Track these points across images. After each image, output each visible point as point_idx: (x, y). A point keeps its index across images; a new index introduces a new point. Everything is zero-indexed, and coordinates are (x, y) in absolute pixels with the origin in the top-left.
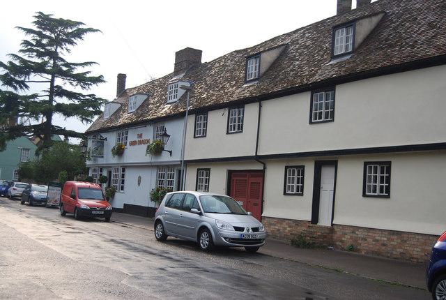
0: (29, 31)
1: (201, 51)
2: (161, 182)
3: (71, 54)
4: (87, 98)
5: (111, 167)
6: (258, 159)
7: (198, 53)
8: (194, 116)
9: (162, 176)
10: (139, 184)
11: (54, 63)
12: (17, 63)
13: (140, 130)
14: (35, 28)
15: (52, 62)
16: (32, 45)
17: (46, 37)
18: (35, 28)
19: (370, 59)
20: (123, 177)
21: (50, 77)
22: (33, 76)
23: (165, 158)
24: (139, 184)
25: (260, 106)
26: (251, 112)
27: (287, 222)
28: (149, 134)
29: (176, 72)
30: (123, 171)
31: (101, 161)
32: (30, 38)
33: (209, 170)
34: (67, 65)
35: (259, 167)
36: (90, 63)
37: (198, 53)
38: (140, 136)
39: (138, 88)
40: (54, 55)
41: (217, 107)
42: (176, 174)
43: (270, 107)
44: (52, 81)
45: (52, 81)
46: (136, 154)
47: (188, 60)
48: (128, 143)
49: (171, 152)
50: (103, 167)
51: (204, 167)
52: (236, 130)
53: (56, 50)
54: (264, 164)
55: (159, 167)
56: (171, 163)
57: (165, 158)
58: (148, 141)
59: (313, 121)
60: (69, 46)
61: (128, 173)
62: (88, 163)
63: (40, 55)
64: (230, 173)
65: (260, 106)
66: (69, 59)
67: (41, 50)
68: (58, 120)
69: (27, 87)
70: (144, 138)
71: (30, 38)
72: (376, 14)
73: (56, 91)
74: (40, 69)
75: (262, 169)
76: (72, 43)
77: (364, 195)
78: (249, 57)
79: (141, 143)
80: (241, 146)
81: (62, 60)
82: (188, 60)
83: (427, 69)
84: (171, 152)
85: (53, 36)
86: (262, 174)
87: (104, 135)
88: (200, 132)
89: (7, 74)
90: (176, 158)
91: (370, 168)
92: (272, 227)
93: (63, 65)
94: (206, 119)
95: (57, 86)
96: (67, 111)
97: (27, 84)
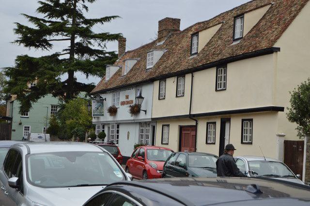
1: (180, 20)
2: (141, 136)
4: (107, 55)
5: (109, 124)
6: (191, 117)
7: (177, 22)
8: (159, 81)
9: (142, 131)
10: (128, 138)
11: (74, 21)
13: (127, 92)
15: (71, 20)
20: (118, 132)
22: (54, 36)
23: (142, 116)
24: (128, 138)
25: (193, 76)
26: (188, 77)
28: (132, 94)
29: (159, 39)
30: (118, 127)
31: (102, 119)
33: (251, 120)
34: (87, 22)
35: (193, 123)
36: (107, 19)
37: (177, 22)
38: (127, 97)
39: (134, 51)
41: (170, 76)
42: (150, 129)
43: (197, 75)
44: (72, 39)
46: (124, 113)
47: (169, 27)
48: (127, 100)
49: (145, 111)
50: (105, 124)
51: (166, 121)
55: (142, 124)
56: (142, 121)
57: (142, 116)
58: (132, 101)
59: (218, 89)
61: (121, 129)
62: (94, 120)
64: (181, 128)
65: (193, 76)
66: (87, 16)
68: (80, 77)
69: (50, 45)
70: (130, 99)
72: (220, 23)
73: (76, 48)
74: (59, 28)
78: (236, 18)
79: (128, 103)
80: (180, 108)
82: (169, 27)
83: (251, 58)
84: (145, 111)
86: (195, 128)
87: (103, 96)
88: (220, 86)
90: (148, 117)
93: (83, 22)
94: (225, 72)
96: (88, 69)
97: (50, 42)
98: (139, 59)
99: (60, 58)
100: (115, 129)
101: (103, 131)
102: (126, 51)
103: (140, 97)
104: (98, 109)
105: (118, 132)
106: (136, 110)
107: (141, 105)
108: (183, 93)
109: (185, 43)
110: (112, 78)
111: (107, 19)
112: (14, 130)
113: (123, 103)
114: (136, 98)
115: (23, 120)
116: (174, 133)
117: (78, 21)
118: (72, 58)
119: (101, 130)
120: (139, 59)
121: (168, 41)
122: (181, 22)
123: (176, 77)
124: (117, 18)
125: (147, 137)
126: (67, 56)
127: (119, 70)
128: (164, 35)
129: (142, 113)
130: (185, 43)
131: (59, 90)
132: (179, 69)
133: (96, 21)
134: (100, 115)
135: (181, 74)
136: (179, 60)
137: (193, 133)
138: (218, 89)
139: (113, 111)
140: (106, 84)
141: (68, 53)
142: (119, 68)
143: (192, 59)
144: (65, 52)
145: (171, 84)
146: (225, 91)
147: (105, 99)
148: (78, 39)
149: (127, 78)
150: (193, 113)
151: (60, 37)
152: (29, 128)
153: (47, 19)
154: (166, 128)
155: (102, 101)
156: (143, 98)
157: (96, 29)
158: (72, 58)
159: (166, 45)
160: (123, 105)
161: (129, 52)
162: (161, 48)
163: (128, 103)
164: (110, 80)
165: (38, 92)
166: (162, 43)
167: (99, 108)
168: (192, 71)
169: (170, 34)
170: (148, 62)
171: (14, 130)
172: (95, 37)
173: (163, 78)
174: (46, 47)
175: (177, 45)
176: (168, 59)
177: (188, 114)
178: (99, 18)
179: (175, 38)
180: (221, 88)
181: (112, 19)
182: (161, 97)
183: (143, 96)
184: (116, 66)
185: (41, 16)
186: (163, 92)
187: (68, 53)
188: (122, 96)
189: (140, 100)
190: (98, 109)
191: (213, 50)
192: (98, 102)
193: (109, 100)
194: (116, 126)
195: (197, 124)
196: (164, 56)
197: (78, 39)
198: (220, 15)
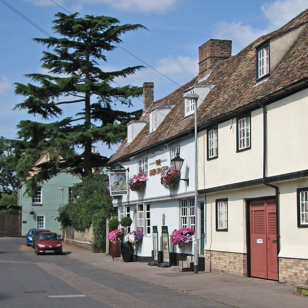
0: (52, 41)
3: (107, 62)
6: (267, 181)
9: (184, 212)
12: (39, 84)
14: (59, 36)
15: (84, 77)
16: (55, 57)
17: (72, 44)
18: (59, 36)
19: (246, 57)
21: (83, 95)
22: (63, 97)
23: (182, 189)
26: (257, 119)
27: (303, 262)
28: (166, 157)
29: (202, 73)
30: (148, 209)
32: (52, 50)
35: (272, 193)
36: (130, 70)
39: (167, 98)
40: (89, 68)
43: (277, 113)
44: (87, 100)
45: (100, 101)
46: (155, 188)
48: (159, 167)
50: (150, 202)
51: (222, 194)
52: (245, 147)
53: (88, 58)
54: (277, 189)
60: (104, 52)
63: (70, 69)
64: (249, 202)
66: (106, 69)
67: (69, 61)
69: (59, 111)
71: (52, 50)
74: (70, 86)
75: (275, 194)
76: (109, 48)
77: (299, 226)
80: (245, 168)
81: (98, 70)
85: (82, 41)
86: (274, 200)
89: (31, 99)
91: (302, 194)
92: (289, 270)
95: (94, 105)
97: (59, 106)
98: (173, 106)
99: (73, 124)
100: (145, 211)
101: (128, 215)
102: (155, 101)
103: (178, 159)
104: (118, 184)
105: (148, 215)
106: (172, 180)
107: (180, 171)
108: (217, 154)
109: (243, 69)
110: (136, 139)
111: (130, 70)
112: (25, 222)
113: (153, 173)
114: (172, 160)
115: (35, 209)
116: (236, 209)
117: (93, 75)
118: (88, 124)
119: (125, 214)
120: (173, 106)
121: (215, 74)
122: (233, 45)
123: (235, 119)
124: (139, 28)
125: (194, 220)
126: (82, 122)
127: (146, 126)
128: (208, 67)
129: (182, 183)
130: (243, 69)
131: (76, 165)
132: (237, 105)
133: (117, 74)
134: (122, 193)
135: (243, 114)
136: (236, 93)
137: (271, 208)
138: (210, 157)
139: (139, 186)
140: (128, 147)
141: (83, 118)
142: (145, 124)
143: (259, 87)
144: (80, 116)
145: (227, 133)
146: (217, 159)
147: (128, 169)
148: (94, 99)
149: (158, 133)
150: (269, 175)
151: (71, 98)
152: (43, 217)
153: (53, 75)
154: (222, 208)
155: (122, 172)
156: (183, 160)
157: (117, 83)
158: (88, 124)
159: (213, 80)
160: (154, 175)
161: (159, 101)
162: (205, 84)
163: (159, 170)
164: (133, 142)
165: (48, 171)
166: (205, 78)
167: (121, 183)
168: (264, 103)
169: (217, 64)
170: (186, 106)
171: (25, 222)
172: (117, 92)
173: (210, 125)
174: (55, 112)
175: (229, 76)
176: (218, 96)
177: (261, 176)
178: (120, 69)
179: (226, 67)
180: (213, 155)
181: (137, 70)
182: (212, 155)
183: (181, 157)
184: (142, 122)
185: (45, 72)
186: (214, 147)
187: (83, 118)
188: (151, 163)
189: (178, 164)
190: (118, 184)
191: (300, 63)
192: (118, 175)
193: (133, 170)
194: (145, 207)
195: (278, 193)
196: (211, 93)
197: (94, 99)
198: (301, 15)
